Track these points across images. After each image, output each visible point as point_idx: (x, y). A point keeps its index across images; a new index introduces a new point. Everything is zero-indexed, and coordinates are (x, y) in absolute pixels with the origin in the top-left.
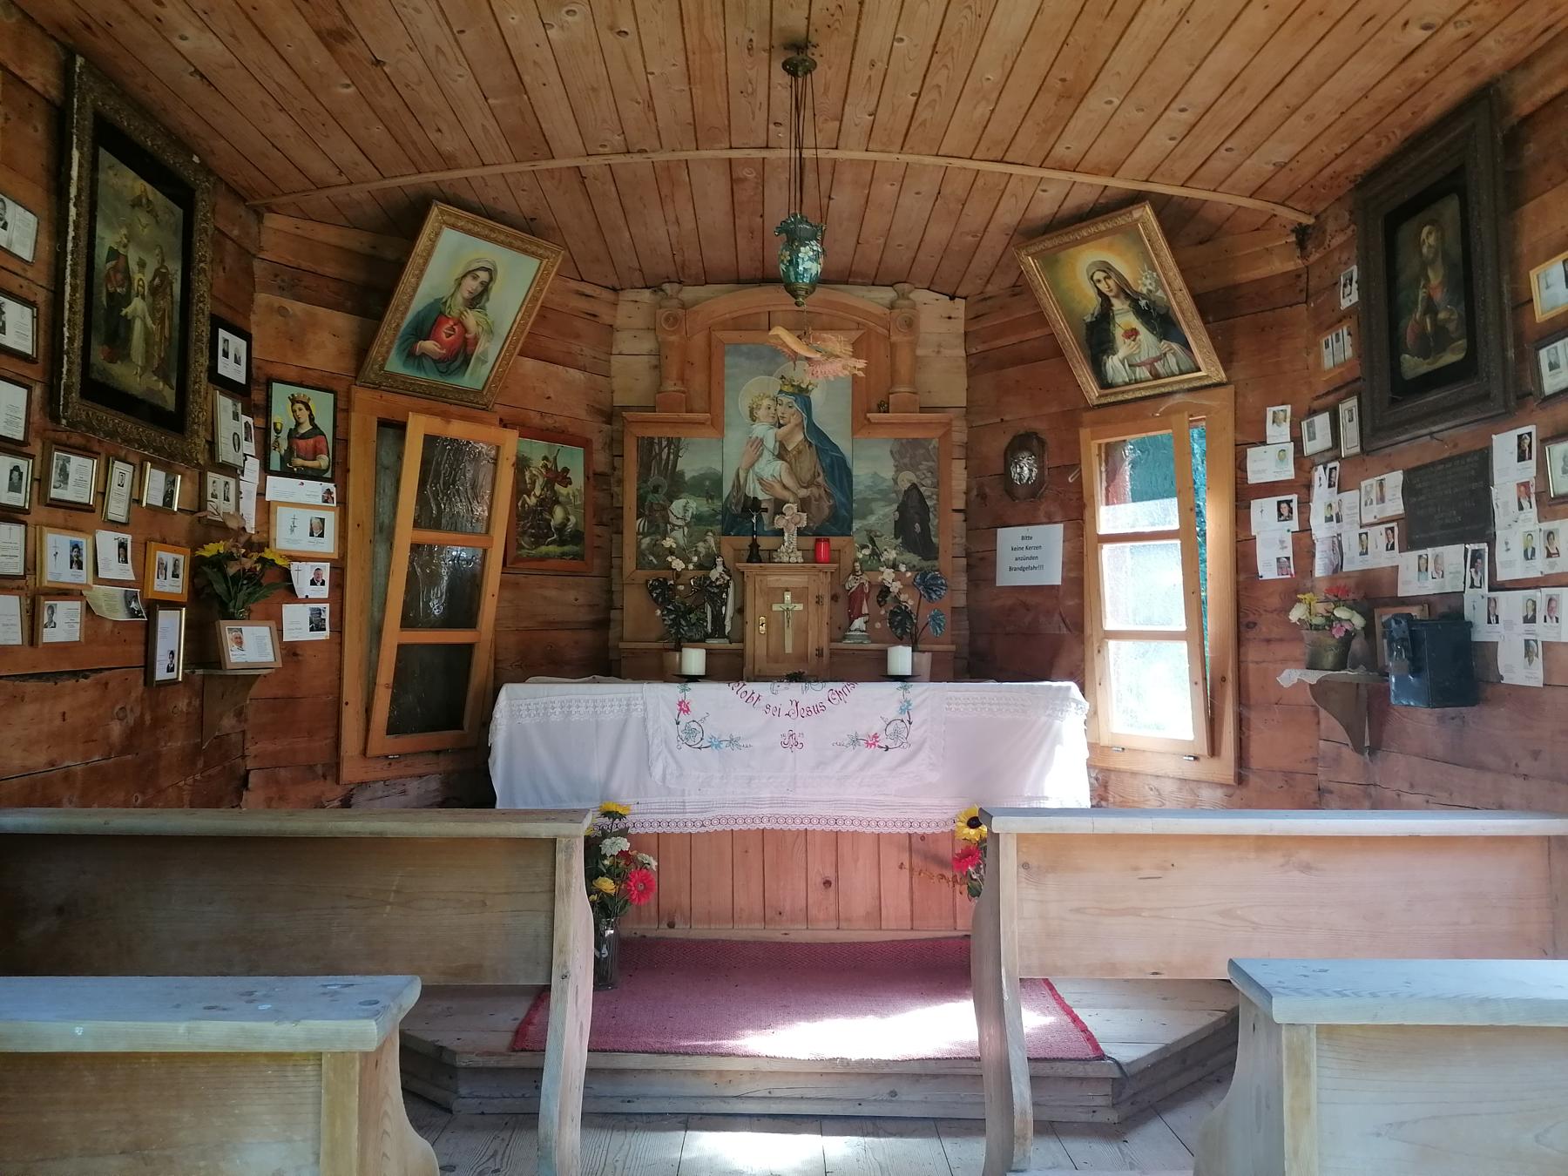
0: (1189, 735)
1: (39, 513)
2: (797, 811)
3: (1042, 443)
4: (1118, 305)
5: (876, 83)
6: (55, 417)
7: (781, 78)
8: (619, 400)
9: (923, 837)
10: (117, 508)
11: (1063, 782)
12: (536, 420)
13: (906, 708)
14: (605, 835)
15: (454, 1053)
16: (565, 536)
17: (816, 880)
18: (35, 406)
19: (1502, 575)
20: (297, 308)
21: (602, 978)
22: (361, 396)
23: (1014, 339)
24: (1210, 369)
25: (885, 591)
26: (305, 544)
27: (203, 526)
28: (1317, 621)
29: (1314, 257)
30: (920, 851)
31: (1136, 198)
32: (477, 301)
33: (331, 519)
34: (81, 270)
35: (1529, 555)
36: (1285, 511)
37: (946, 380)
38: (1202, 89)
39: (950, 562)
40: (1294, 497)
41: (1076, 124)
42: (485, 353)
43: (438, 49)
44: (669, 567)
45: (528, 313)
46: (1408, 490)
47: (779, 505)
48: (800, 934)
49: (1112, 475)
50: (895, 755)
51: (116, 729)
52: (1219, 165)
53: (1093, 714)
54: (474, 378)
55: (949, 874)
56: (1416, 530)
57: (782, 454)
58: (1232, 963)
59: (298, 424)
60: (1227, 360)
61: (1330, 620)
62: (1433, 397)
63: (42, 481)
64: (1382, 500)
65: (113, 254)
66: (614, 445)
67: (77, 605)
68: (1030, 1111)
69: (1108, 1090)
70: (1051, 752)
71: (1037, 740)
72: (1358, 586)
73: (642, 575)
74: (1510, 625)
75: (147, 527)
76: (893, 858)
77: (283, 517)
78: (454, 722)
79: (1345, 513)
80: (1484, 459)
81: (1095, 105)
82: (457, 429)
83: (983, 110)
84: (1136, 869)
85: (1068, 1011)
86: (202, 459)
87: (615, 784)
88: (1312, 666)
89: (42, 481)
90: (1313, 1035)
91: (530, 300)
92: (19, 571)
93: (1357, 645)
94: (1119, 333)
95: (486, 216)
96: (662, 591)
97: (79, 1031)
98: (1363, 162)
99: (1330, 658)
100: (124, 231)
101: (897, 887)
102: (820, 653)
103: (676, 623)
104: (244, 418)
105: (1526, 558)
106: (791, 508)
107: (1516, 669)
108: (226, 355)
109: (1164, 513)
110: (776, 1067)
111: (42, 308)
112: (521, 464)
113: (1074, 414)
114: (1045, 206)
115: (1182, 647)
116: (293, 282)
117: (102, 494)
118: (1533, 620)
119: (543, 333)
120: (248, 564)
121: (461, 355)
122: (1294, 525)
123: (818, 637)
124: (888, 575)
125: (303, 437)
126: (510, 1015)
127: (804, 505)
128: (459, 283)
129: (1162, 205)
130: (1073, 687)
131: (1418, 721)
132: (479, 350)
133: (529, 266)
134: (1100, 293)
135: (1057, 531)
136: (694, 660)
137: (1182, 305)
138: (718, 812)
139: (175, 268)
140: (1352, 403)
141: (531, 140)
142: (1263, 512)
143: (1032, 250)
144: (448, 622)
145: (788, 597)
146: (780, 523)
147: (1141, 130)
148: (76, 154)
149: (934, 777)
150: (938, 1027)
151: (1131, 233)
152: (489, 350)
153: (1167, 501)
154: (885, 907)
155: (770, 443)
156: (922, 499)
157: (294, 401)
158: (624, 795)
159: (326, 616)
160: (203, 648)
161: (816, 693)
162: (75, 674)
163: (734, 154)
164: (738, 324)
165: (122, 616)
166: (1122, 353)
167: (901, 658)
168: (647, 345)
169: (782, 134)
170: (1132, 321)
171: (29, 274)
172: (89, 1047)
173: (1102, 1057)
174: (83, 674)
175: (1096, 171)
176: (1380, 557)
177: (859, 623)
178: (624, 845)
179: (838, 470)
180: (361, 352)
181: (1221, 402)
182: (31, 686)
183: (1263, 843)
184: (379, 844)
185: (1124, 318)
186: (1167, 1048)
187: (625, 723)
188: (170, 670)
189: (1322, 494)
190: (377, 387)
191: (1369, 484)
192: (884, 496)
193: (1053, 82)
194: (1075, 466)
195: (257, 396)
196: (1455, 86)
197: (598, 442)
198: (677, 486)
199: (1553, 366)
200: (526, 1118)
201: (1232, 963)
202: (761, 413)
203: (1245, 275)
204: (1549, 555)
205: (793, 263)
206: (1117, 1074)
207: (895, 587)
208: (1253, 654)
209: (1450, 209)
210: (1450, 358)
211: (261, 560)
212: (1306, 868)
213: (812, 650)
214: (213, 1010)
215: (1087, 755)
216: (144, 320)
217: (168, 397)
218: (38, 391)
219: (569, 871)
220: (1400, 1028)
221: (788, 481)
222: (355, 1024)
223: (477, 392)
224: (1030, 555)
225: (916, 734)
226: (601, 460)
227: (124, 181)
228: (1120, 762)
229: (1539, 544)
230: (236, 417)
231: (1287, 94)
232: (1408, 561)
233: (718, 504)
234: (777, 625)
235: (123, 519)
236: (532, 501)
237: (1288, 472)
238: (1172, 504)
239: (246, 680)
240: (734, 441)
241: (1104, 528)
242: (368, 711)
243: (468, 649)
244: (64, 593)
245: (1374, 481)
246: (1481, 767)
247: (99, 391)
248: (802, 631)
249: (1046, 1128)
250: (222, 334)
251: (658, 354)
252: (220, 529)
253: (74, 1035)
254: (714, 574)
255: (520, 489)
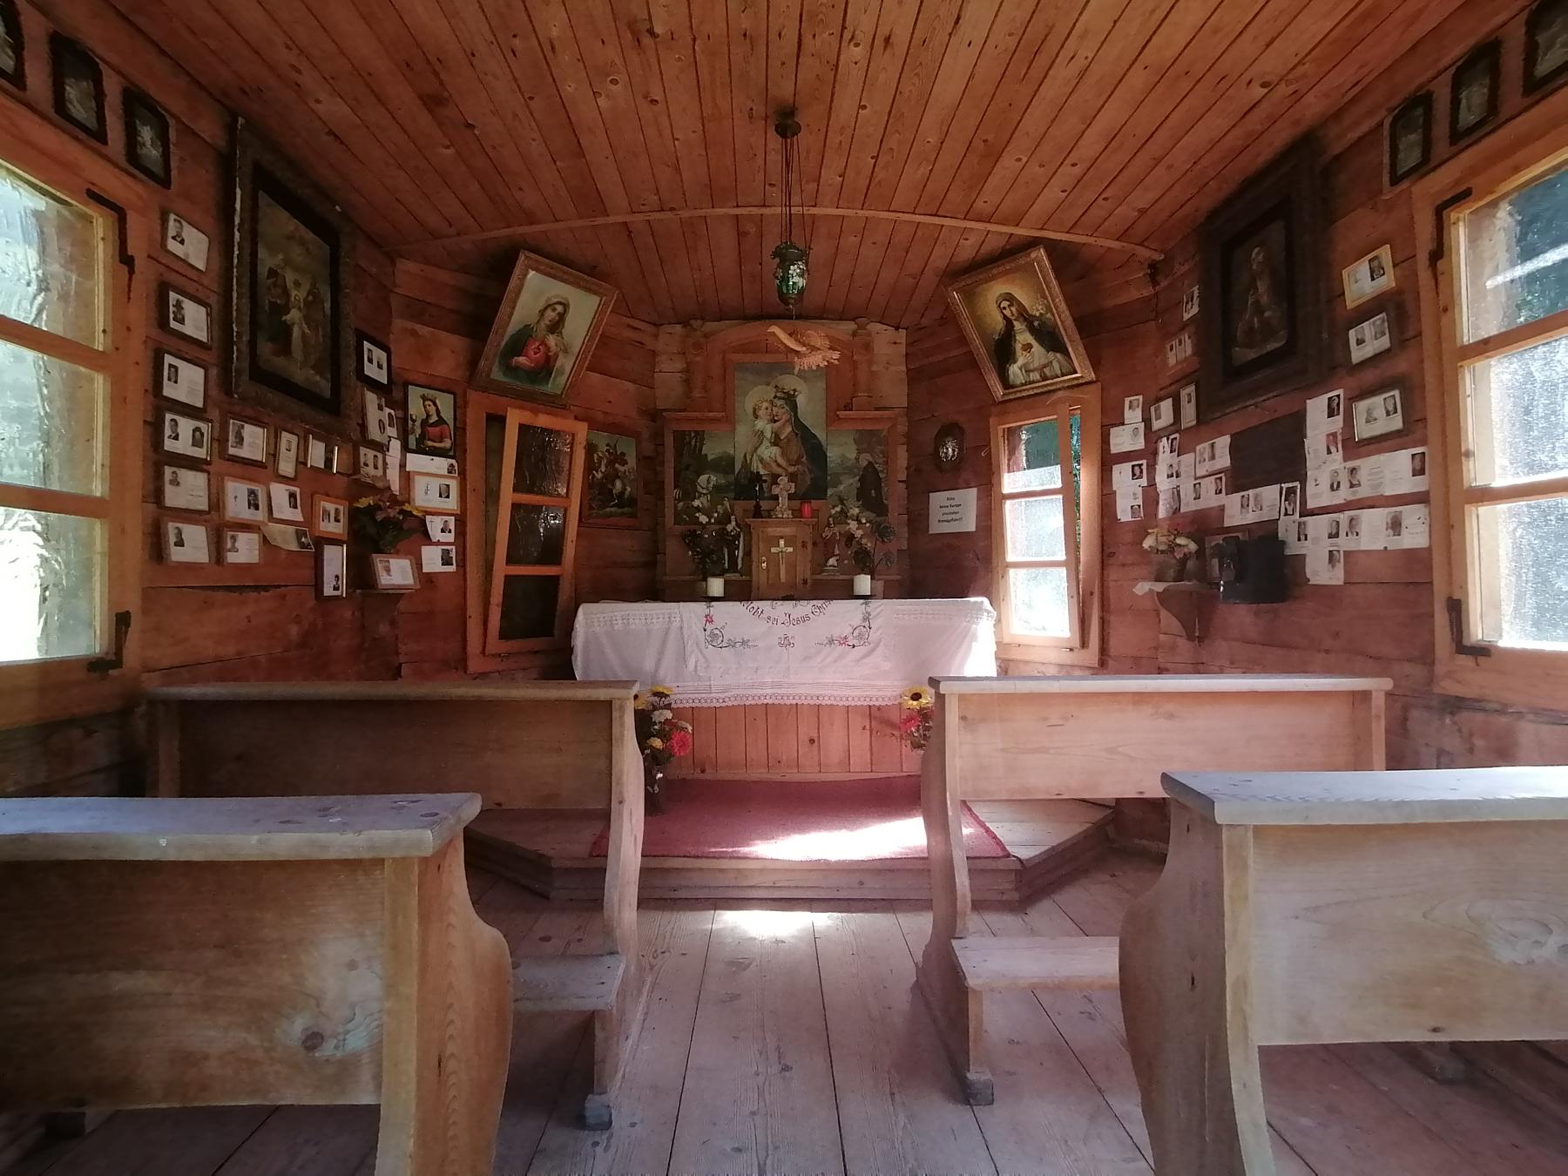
0: (1066, 633)
1: (218, 465)
2: (791, 691)
3: (961, 430)
4: (1018, 325)
5: (846, 146)
6: (228, 393)
7: (775, 141)
8: (660, 405)
9: (879, 708)
10: (287, 467)
11: (978, 661)
12: (600, 416)
13: (867, 618)
14: (655, 708)
15: (550, 858)
16: (623, 502)
17: (804, 738)
18: (212, 384)
19: (1311, 505)
20: (424, 330)
21: (653, 805)
22: (473, 396)
23: (940, 357)
24: (1084, 371)
25: (850, 537)
26: (436, 502)
27: (356, 485)
28: (1162, 548)
29: (1164, 284)
30: (876, 716)
31: (1033, 243)
32: (556, 327)
33: (454, 485)
34: (246, 280)
35: (1334, 487)
36: (1137, 470)
37: (893, 389)
38: (1091, 144)
39: (896, 517)
40: (1144, 462)
41: (993, 181)
42: (562, 366)
43: (515, 115)
44: (696, 521)
45: (592, 338)
46: (1234, 449)
47: (775, 478)
48: (793, 776)
49: (1012, 452)
50: (860, 651)
51: (294, 630)
52: (1097, 213)
53: (999, 621)
54: (556, 384)
55: (897, 733)
56: (1239, 478)
57: (776, 441)
58: (1166, 779)
59: (428, 416)
60: (1096, 364)
61: (1172, 547)
62: (1259, 376)
63: (221, 441)
64: (1213, 457)
65: (273, 273)
66: (658, 437)
67: (255, 536)
68: (969, 895)
69: (1013, 877)
70: (969, 648)
71: (965, 638)
72: (1193, 522)
73: (679, 529)
74: (1316, 540)
75: (310, 483)
76: (858, 722)
77: (419, 484)
78: (549, 632)
79: (1182, 471)
80: (1297, 424)
81: (1008, 164)
82: (543, 421)
83: (924, 170)
84: (1045, 719)
85: (982, 824)
86: (355, 435)
87: (662, 673)
88: (1158, 579)
89: (221, 441)
90: (1250, 834)
91: (594, 327)
92: (205, 507)
93: (1190, 564)
94: (1018, 347)
95: (561, 263)
96: (691, 538)
97: (163, 842)
98: (1207, 203)
99: (1171, 573)
100: (281, 257)
101: (860, 743)
102: (805, 582)
103: (702, 561)
104: (388, 410)
105: (1332, 489)
106: (783, 480)
107: (1321, 572)
108: (370, 361)
109: (1051, 476)
110: (779, 866)
111: (215, 307)
112: (590, 448)
113: (987, 408)
114: (967, 251)
115: (1063, 572)
116: (418, 311)
117: (274, 455)
118: (1337, 535)
119: (603, 352)
120: (392, 513)
121: (545, 369)
122: (1144, 482)
123: (804, 571)
124: (853, 525)
125: (434, 425)
126: (588, 834)
127: (793, 477)
128: (542, 313)
129: (1052, 247)
130: (986, 601)
131: (1240, 617)
132: (558, 364)
133: (594, 301)
134: (1005, 317)
135: (972, 493)
136: (716, 586)
137: (1063, 320)
138: (735, 692)
139: (325, 291)
140: (1191, 389)
141: (591, 200)
142: (1122, 475)
143: (957, 285)
144: (541, 561)
145: (782, 542)
146: (776, 490)
147: (1040, 188)
148: (238, 191)
149: (887, 666)
150: (899, 836)
151: (1028, 270)
152: (565, 364)
153: (1051, 469)
154: (848, 755)
155: (768, 434)
156: (876, 472)
157: (424, 398)
158: (669, 683)
159: (453, 555)
160: (361, 574)
161: (804, 608)
162: (256, 588)
163: (739, 211)
164: (743, 349)
165: (294, 547)
166: (1021, 361)
167: (864, 583)
168: (679, 365)
169: (775, 194)
170: (1030, 339)
171: (206, 282)
172: (172, 856)
173: (1008, 855)
174: (266, 588)
175: (1004, 222)
176: (1210, 498)
177: (832, 561)
178: (668, 715)
179: (815, 452)
180: (473, 364)
181: (1092, 396)
182: (220, 595)
183: (1140, 698)
184: (480, 704)
185: (1023, 336)
186: (1053, 848)
187: (667, 633)
188: (336, 588)
189: (1165, 457)
190: (484, 390)
191: (1203, 447)
192: (849, 471)
193: (977, 143)
194: (987, 445)
195: (397, 394)
196: (1281, 136)
197: (645, 435)
198: (703, 465)
199: (1360, 342)
200: (595, 902)
201: (1166, 779)
202: (761, 413)
203: (1110, 303)
204: (1352, 486)
205: (785, 279)
206: (1019, 867)
207: (859, 533)
208: (1113, 574)
209: (1276, 232)
210: (1273, 346)
211: (402, 512)
212: (1171, 716)
213: (799, 580)
214: (286, 823)
215: (994, 648)
216: (301, 328)
217: (324, 387)
218: (214, 372)
219: (622, 725)
220: (1328, 827)
221: (780, 460)
222: (412, 831)
223: (555, 395)
224: (954, 511)
225: (874, 636)
226: (648, 448)
227: (279, 221)
228: (1016, 654)
229: (1344, 478)
230: (380, 408)
231: (1153, 148)
232: (1233, 502)
233: (731, 478)
234: (774, 561)
235: (291, 475)
236: (599, 476)
237: (1140, 444)
238: (1056, 470)
239: (394, 596)
240: (742, 432)
241: (1006, 490)
242: (485, 622)
243: (555, 579)
244: (246, 527)
245: (1207, 445)
246: (1285, 646)
247: (259, 374)
248: (792, 567)
249: (978, 906)
250: (366, 345)
251: (687, 370)
252: (371, 489)
253: (158, 846)
254: (729, 528)
255: (590, 467)
